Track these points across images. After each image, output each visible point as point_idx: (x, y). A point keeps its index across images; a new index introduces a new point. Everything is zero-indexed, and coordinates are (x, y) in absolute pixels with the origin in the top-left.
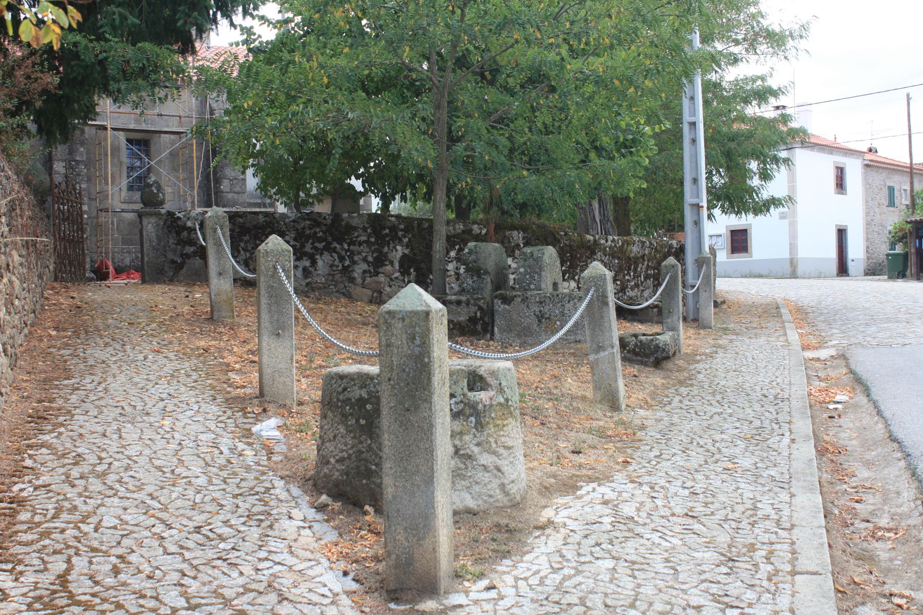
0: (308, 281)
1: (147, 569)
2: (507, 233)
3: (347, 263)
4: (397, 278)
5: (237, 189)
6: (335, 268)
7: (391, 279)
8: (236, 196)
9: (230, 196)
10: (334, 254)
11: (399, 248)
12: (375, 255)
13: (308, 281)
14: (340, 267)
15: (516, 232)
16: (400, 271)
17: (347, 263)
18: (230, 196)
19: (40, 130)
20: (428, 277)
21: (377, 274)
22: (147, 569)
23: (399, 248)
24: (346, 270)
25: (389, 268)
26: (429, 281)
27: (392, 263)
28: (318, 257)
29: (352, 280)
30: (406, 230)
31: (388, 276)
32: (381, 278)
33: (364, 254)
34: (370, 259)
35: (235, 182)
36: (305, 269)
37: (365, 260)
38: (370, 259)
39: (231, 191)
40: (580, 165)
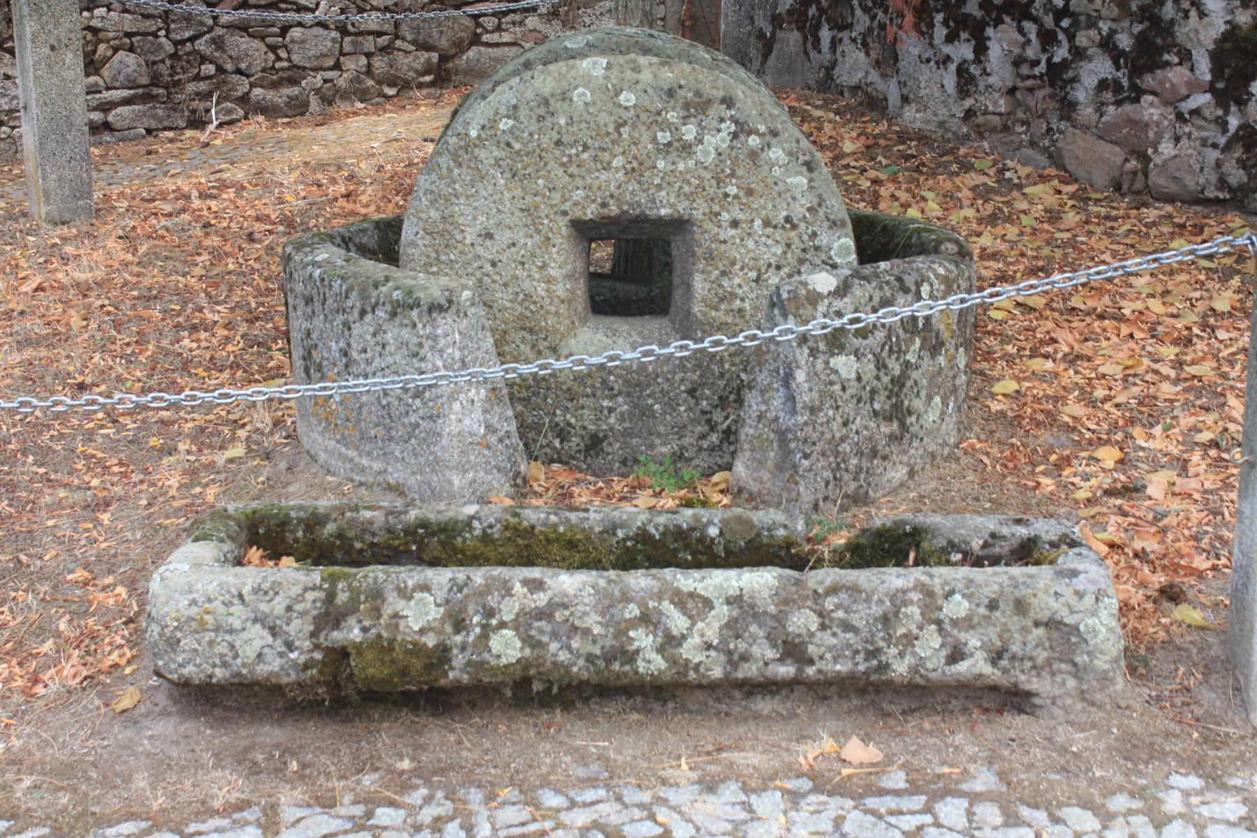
0: (968, 103)
3: (1061, 53)
4: (1196, 112)
6: (1025, 70)
7: (1180, 116)
10: (1029, 26)
12: (1137, 28)
13: (968, 103)
14: (1042, 68)
16: (1211, 89)
17: (1061, 53)
19: (425, 784)
21: (1137, 94)
24: (1058, 76)
25: (1176, 75)
27: (1186, 57)
28: (990, 31)
29: (1068, 108)
31: (1171, 100)
32: (1150, 110)
33: (1105, 27)
34: (1124, 42)
36: (962, 71)
37: (1108, 45)
38: (1124, 42)
40: (502, 145)
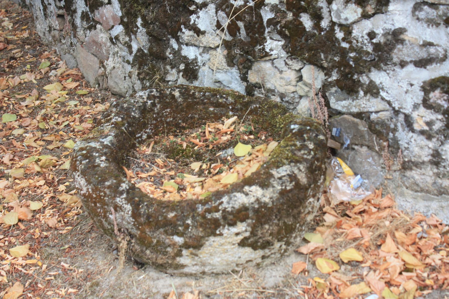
4: (117, 38)
20: (168, 45)
26: (169, 54)
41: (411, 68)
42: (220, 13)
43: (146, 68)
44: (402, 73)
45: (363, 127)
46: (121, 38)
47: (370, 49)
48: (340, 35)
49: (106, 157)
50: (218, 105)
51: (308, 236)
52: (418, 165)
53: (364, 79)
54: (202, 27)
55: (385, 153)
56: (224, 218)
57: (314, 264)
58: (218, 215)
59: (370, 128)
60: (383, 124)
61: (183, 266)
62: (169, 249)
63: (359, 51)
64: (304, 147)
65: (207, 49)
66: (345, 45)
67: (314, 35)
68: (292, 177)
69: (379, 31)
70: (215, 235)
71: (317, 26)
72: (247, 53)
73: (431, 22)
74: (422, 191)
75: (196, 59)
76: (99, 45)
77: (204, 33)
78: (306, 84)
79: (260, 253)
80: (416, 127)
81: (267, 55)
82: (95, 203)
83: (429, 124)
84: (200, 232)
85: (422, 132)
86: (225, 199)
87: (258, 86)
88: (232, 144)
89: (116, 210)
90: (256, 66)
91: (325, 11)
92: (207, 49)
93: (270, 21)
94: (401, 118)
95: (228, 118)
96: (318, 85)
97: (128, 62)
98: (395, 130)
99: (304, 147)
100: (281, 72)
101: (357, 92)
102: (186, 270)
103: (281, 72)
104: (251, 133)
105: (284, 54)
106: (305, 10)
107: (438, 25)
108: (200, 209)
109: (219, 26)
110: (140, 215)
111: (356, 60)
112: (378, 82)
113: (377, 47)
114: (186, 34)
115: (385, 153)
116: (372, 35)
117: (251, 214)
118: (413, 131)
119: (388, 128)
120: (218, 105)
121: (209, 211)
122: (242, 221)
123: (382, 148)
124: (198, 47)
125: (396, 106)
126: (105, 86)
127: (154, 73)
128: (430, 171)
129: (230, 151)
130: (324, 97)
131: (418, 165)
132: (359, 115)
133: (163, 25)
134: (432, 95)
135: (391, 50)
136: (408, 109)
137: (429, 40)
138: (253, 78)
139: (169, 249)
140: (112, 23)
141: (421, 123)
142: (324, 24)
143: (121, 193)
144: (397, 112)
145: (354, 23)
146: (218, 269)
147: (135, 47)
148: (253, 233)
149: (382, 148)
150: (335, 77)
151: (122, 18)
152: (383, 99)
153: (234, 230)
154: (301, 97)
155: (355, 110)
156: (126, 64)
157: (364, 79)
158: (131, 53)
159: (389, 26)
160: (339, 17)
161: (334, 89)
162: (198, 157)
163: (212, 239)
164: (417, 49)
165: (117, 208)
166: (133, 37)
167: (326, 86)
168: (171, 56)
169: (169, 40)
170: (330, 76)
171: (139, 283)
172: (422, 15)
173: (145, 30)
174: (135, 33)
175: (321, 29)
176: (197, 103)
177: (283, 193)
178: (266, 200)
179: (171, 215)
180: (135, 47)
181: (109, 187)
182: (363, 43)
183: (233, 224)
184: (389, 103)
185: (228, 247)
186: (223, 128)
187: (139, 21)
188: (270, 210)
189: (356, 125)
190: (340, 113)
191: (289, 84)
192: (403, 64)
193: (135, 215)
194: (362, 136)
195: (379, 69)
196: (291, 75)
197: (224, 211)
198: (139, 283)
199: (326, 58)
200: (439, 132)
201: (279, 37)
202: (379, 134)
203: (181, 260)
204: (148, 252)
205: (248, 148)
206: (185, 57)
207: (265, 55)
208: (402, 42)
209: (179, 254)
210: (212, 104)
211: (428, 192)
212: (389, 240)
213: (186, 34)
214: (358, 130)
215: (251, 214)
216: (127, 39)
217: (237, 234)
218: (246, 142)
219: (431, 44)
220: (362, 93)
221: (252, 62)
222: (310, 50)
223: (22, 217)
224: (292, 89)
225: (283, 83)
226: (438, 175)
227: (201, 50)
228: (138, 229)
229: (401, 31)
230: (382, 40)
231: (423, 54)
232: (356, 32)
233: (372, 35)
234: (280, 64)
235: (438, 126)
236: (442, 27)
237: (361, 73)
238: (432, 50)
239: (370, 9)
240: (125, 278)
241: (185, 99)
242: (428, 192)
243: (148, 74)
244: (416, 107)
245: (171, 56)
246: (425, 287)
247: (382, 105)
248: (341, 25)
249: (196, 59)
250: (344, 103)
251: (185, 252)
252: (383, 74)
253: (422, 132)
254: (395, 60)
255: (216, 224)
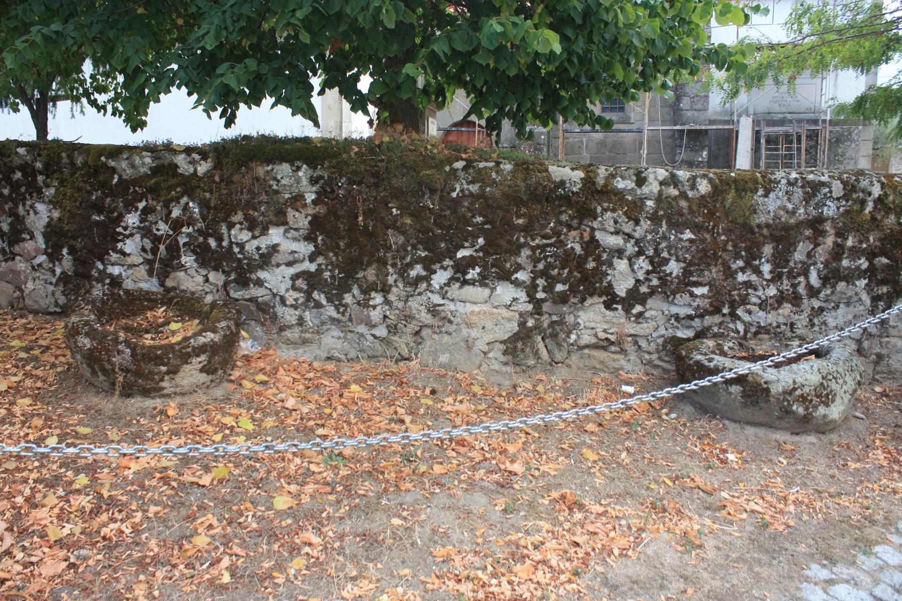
1: (617, 481)
2: (261, 170)
4: (40, 265)
5: (699, 106)
8: (696, 113)
9: (690, 114)
11: (40, 207)
15: (284, 169)
16: (45, 253)
18: (690, 114)
20: (93, 266)
22: (617, 481)
23: (40, 207)
26: (94, 273)
30: (48, 171)
32: (20, 265)
35: (696, 99)
39: (691, 109)
41: (283, 267)
42: (145, 240)
43: (71, 286)
44: (278, 271)
45: (253, 307)
46: (44, 265)
47: (257, 257)
48: (236, 250)
49: (325, 216)
50: (150, 300)
51: (232, 372)
52: (290, 327)
53: (253, 276)
54: (127, 251)
55: (268, 323)
56: (193, 351)
57: (241, 385)
58: (189, 350)
59: (257, 308)
60: (266, 304)
61: (164, 388)
62: (156, 377)
63: (250, 259)
64: (230, 312)
65: (131, 266)
66: (239, 256)
67: (217, 251)
68: (228, 327)
69: (263, 246)
70: (187, 363)
71: (220, 245)
72: (167, 266)
73: (295, 239)
74: (292, 343)
75: (120, 274)
76: (17, 273)
77: (129, 255)
78: (211, 284)
79: (210, 377)
80: (288, 303)
81: (183, 266)
82: (100, 353)
83: (296, 300)
84: (178, 362)
85: (292, 306)
86: (192, 341)
87: (174, 289)
88: (167, 323)
89: (118, 354)
90: (172, 275)
91: (226, 236)
92: (131, 266)
93: (185, 244)
94: (278, 298)
95: (159, 308)
96: (220, 283)
97: (51, 283)
98: (274, 307)
99: (230, 312)
100: (192, 277)
101: (249, 285)
102: (165, 391)
103: (192, 277)
104: (178, 316)
105: (195, 265)
106: (211, 236)
107: (299, 241)
108: (177, 347)
109: (144, 250)
110: (137, 355)
111: (248, 264)
112: (262, 277)
113: (262, 256)
114: (114, 256)
115: (268, 323)
116: (258, 248)
117: (209, 349)
118: (286, 306)
119: (269, 306)
120: (150, 300)
121: (184, 348)
122: (204, 353)
123: (266, 320)
124: (123, 265)
125: (275, 291)
126: (21, 305)
127: (80, 289)
128: (297, 329)
129: (166, 327)
130: (225, 290)
131: (290, 327)
132: (250, 300)
133: (91, 252)
134: (297, 282)
135: (271, 256)
136: (282, 292)
137: (294, 249)
138: (169, 283)
139: (156, 377)
140: (34, 254)
141: (291, 300)
142: (225, 244)
143: (121, 343)
144: (275, 295)
145: (246, 242)
146: (186, 389)
147: (58, 271)
148: (209, 362)
149: (266, 320)
150: (233, 277)
151: (45, 249)
152: (266, 288)
153: (199, 359)
154: (206, 293)
155: (247, 297)
156: (48, 286)
157: (253, 276)
158: (54, 275)
159: (269, 243)
160: (236, 238)
161: (232, 285)
162: (147, 332)
163: (185, 366)
164: (287, 255)
165: (119, 352)
166: (57, 263)
167: (226, 284)
168: (96, 275)
169: (94, 263)
170: (229, 276)
171: (132, 405)
172: (289, 235)
173: (70, 257)
174: (60, 260)
175: (223, 247)
176: (136, 300)
177: (225, 336)
178: (216, 340)
179: (159, 352)
180: (58, 271)
181: (111, 340)
182: (252, 254)
183: (198, 356)
184: (270, 290)
185: (194, 372)
186: (159, 314)
187: (65, 251)
188: (219, 346)
189: (248, 306)
190: (237, 300)
191: (198, 285)
192: (278, 265)
193: (134, 355)
194: (252, 314)
195: (262, 268)
196: (200, 279)
197: (193, 347)
198: (132, 405)
199: (227, 265)
200: (302, 304)
201: (191, 254)
202: (264, 311)
203: (163, 384)
204: (140, 381)
205: (180, 324)
206: (111, 274)
207: (181, 267)
208: (278, 251)
209: (162, 380)
210: (146, 300)
211: (296, 343)
212: (281, 369)
213: (114, 256)
214: (250, 310)
215: (209, 349)
216: (51, 265)
217: (200, 362)
218: (177, 322)
219: (296, 252)
220: (252, 285)
221: (169, 273)
222: (215, 260)
223: (10, 385)
224: (201, 288)
225: (194, 284)
226: (302, 332)
227: (125, 267)
228: (135, 365)
229: (277, 245)
230: (265, 251)
231: (291, 258)
232: (247, 247)
233: (258, 248)
234: (192, 272)
235: (301, 301)
236: (302, 241)
237: (251, 272)
238: (296, 255)
239: (257, 233)
240: (119, 404)
241: (128, 297)
242: (296, 343)
243: (73, 290)
244: (287, 290)
245: (96, 275)
246: (308, 388)
247: (265, 292)
248: (237, 244)
249: (120, 274)
250: (239, 293)
251: (166, 378)
252: (266, 272)
253: (292, 306)
254: (273, 263)
255: (189, 355)
